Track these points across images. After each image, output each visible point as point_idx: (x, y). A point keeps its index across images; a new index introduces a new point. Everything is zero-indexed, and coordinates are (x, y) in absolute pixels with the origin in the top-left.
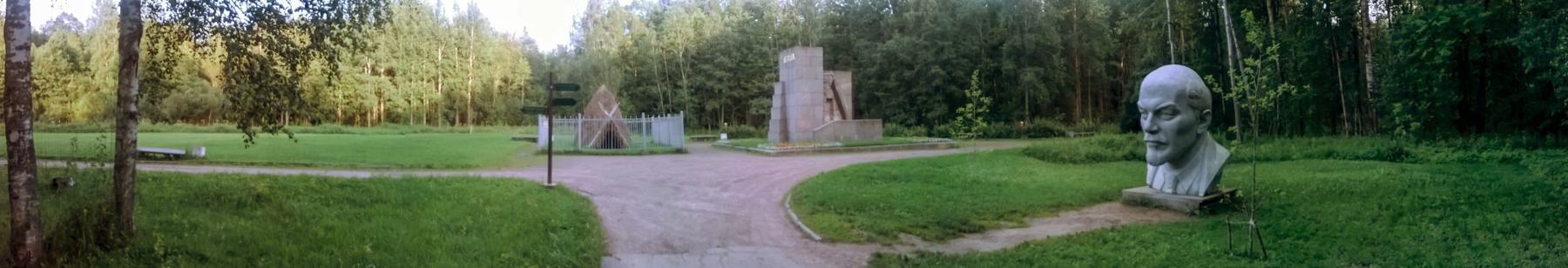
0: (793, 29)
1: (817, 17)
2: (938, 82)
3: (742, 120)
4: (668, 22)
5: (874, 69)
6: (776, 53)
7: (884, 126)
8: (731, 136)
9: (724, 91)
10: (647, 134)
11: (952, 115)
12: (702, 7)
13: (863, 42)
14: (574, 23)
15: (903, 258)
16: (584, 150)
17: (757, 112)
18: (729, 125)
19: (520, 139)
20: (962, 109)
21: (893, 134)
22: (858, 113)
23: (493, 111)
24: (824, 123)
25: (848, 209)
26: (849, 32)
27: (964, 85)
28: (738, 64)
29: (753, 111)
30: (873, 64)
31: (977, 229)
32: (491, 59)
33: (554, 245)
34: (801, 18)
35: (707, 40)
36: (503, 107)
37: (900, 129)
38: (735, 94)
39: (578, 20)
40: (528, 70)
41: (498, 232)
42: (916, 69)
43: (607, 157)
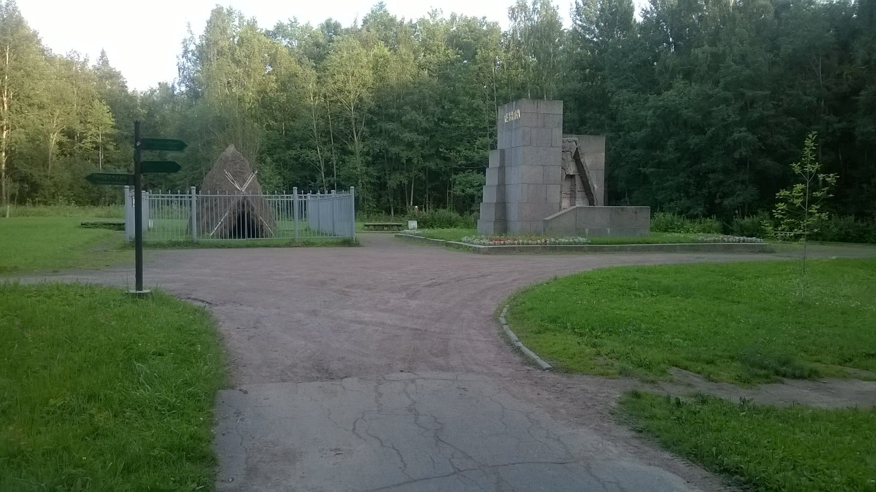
0: (520, 76)
1: (558, 59)
2: (743, 151)
3: (440, 203)
4: (334, 58)
5: (644, 132)
6: (492, 109)
7: (652, 217)
8: (422, 224)
9: (415, 161)
10: (301, 217)
11: (767, 201)
12: (386, 40)
13: (625, 94)
14: (186, 52)
15: (673, 401)
16: (201, 240)
17: (463, 191)
18: (420, 209)
19: (95, 225)
20: (783, 193)
21: (667, 228)
22: (614, 197)
23: (49, 182)
24: (560, 209)
25: (593, 329)
26: (604, 78)
27: (785, 158)
28: (436, 124)
29: (457, 190)
30: (642, 126)
31: (806, 374)
32: (45, 100)
33: (141, 379)
34: (532, 59)
35: (392, 87)
36: (67, 176)
37: (678, 221)
38: (432, 165)
39: (192, 47)
40: (108, 119)
41: (45, 368)
42: (709, 133)
43: (238, 250)
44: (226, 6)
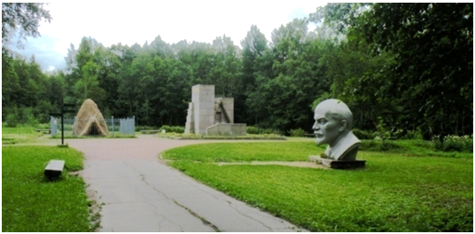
22: (236, 121)
42: (277, 80)
44: (87, 36)
